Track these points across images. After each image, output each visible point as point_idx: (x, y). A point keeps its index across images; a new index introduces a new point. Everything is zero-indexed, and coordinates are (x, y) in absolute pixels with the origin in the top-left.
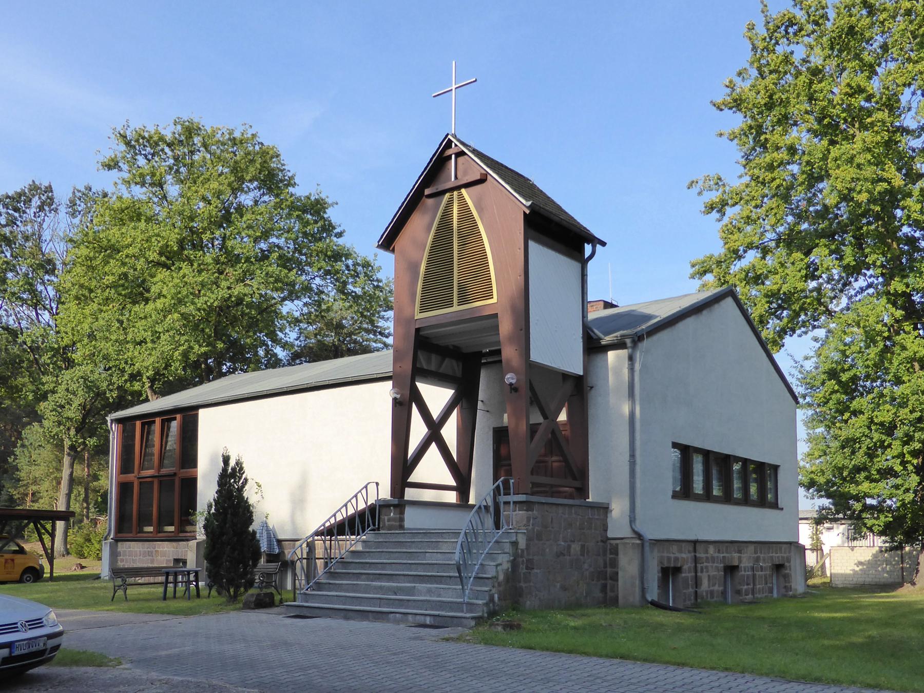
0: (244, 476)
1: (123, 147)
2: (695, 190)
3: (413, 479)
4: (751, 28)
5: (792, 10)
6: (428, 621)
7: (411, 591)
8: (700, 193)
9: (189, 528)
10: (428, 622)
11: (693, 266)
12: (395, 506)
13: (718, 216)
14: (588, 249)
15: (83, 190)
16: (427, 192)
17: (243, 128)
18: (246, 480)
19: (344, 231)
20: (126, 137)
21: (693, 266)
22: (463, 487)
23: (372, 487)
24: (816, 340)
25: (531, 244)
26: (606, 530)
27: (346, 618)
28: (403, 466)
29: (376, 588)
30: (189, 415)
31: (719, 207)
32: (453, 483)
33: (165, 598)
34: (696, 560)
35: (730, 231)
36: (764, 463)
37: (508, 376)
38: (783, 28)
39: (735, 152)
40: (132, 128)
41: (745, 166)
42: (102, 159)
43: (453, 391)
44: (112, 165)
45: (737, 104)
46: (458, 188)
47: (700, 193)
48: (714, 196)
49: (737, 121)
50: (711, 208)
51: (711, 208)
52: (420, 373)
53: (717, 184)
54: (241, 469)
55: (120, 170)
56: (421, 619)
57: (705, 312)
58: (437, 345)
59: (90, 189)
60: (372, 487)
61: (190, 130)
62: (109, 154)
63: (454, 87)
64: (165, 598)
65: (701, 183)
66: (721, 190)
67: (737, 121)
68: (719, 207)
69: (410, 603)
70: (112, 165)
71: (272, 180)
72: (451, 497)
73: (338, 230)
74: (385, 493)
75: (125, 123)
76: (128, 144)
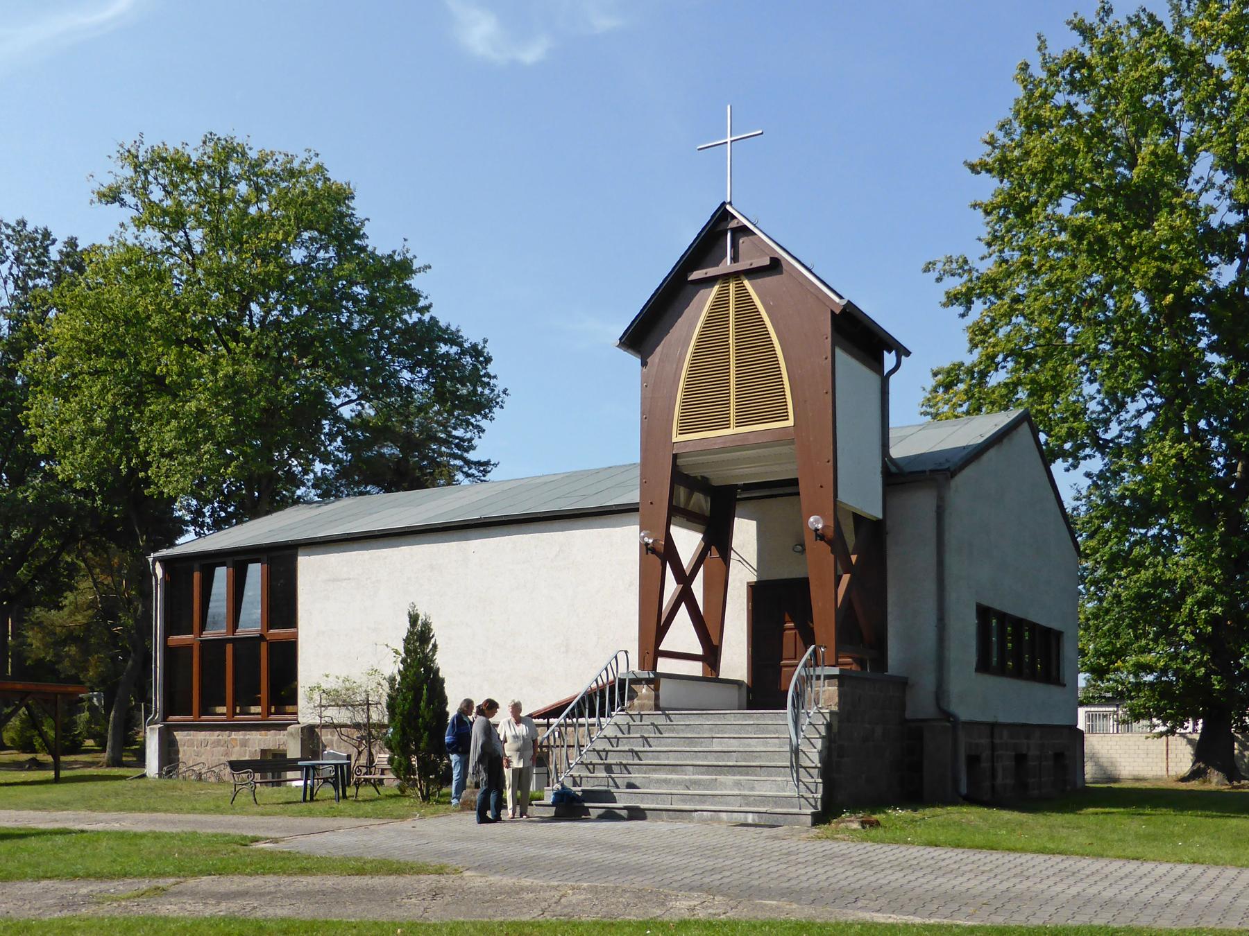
0: (433, 641)
1: (129, 172)
2: (934, 275)
3: (663, 647)
4: (1025, 67)
5: (1081, 50)
6: (750, 818)
7: (707, 784)
8: (939, 280)
9: (290, 708)
10: (750, 821)
11: (935, 375)
12: (648, 681)
13: (961, 310)
14: (889, 359)
15: (13, 224)
16: (696, 275)
17: (306, 155)
18: (435, 646)
19: (431, 305)
20: (137, 157)
21: (935, 375)
22: (711, 655)
23: (622, 657)
24: (1088, 475)
25: (838, 351)
26: (904, 710)
27: (672, 819)
28: (654, 627)
29: (658, 781)
30: (281, 561)
31: (964, 299)
32: (699, 651)
33: (305, 800)
34: (993, 747)
35: (980, 334)
36: (1050, 629)
37: (812, 519)
38: (1068, 71)
39: (981, 226)
40: (147, 146)
41: (989, 245)
42: (96, 187)
43: (701, 536)
44: (112, 196)
45: (1003, 167)
46: (737, 275)
47: (939, 280)
48: (956, 284)
49: (989, 187)
50: (952, 299)
51: (952, 299)
52: (677, 512)
53: (961, 267)
54: (430, 630)
55: (123, 204)
56: (741, 817)
57: (1005, 441)
58: (687, 476)
59: (25, 225)
60: (622, 657)
61: (229, 151)
62: (109, 181)
63: (729, 140)
64: (305, 800)
65: (939, 266)
66: (966, 277)
67: (989, 187)
68: (964, 299)
69: (716, 799)
70: (112, 196)
71: (344, 234)
72: (696, 669)
73: (422, 303)
74: (631, 665)
75: (138, 138)
76: (137, 167)
